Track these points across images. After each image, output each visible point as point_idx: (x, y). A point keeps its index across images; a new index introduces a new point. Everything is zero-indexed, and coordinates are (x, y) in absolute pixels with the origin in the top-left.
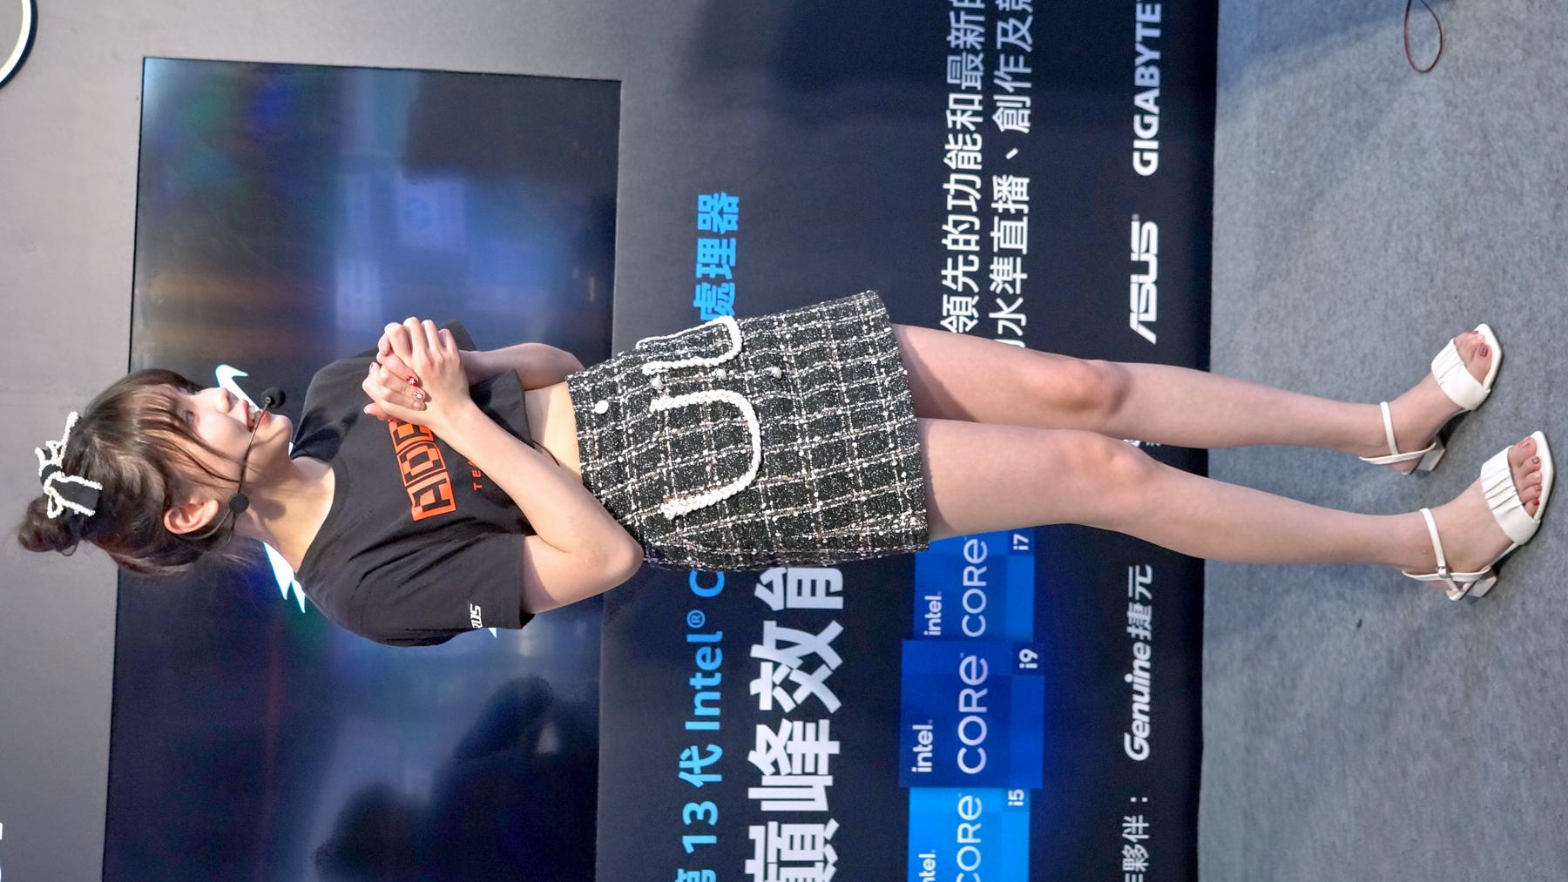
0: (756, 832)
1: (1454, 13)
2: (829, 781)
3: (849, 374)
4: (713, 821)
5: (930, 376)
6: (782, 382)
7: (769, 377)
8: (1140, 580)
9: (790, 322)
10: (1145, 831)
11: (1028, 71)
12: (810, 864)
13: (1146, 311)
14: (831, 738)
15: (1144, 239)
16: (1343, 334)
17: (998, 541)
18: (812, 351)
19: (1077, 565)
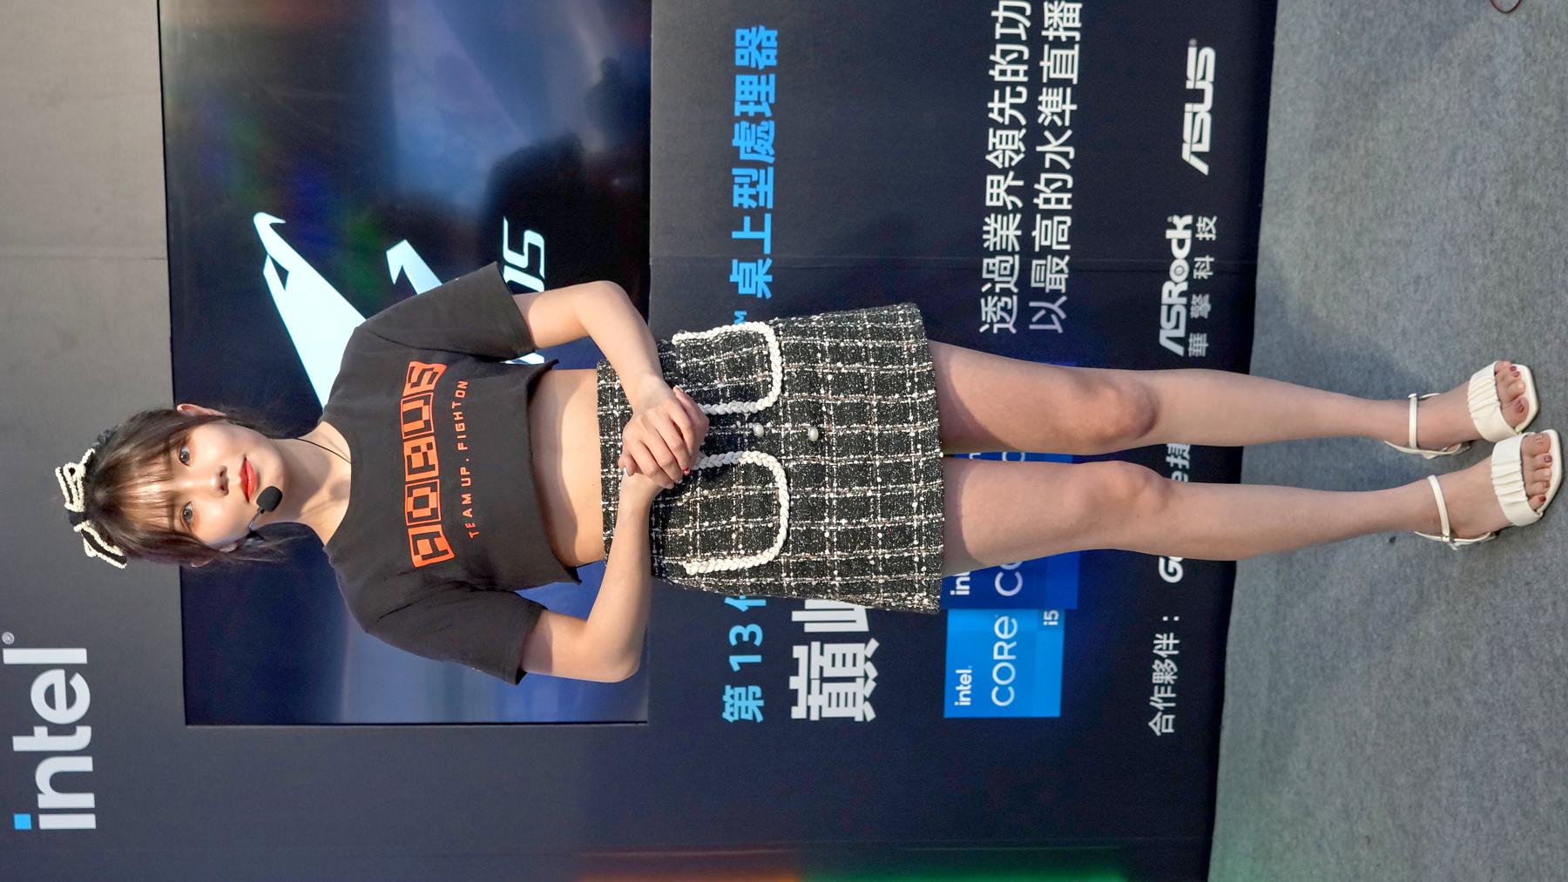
0: (799, 652)
3: (886, 444)
4: (758, 642)
10: (1175, 647)
12: (852, 679)
13: (1200, 141)
15: (1201, 66)
16: (1399, 242)
18: (851, 404)
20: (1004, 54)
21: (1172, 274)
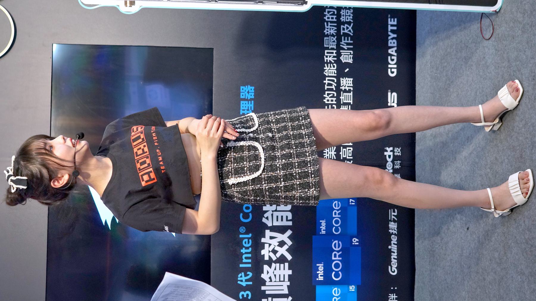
1: (497, 19)
2: (288, 283)
3: (295, 137)
5: (324, 139)
6: (272, 139)
7: (268, 136)
8: (393, 214)
9: (275, 114)
11: (352, 42)
14: (289, 269)
17: (345, 201)
18: (282, 127)
19: (371, 212)
20: (328, 94)
21: (387, 167)
